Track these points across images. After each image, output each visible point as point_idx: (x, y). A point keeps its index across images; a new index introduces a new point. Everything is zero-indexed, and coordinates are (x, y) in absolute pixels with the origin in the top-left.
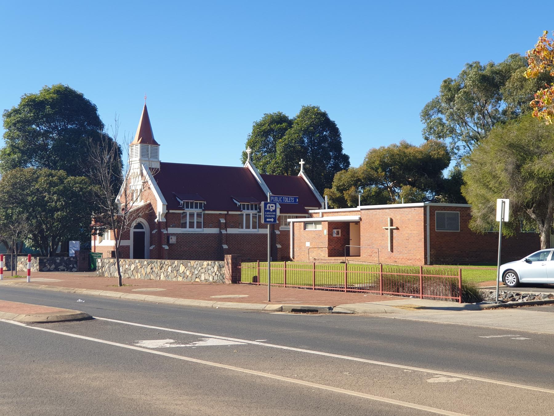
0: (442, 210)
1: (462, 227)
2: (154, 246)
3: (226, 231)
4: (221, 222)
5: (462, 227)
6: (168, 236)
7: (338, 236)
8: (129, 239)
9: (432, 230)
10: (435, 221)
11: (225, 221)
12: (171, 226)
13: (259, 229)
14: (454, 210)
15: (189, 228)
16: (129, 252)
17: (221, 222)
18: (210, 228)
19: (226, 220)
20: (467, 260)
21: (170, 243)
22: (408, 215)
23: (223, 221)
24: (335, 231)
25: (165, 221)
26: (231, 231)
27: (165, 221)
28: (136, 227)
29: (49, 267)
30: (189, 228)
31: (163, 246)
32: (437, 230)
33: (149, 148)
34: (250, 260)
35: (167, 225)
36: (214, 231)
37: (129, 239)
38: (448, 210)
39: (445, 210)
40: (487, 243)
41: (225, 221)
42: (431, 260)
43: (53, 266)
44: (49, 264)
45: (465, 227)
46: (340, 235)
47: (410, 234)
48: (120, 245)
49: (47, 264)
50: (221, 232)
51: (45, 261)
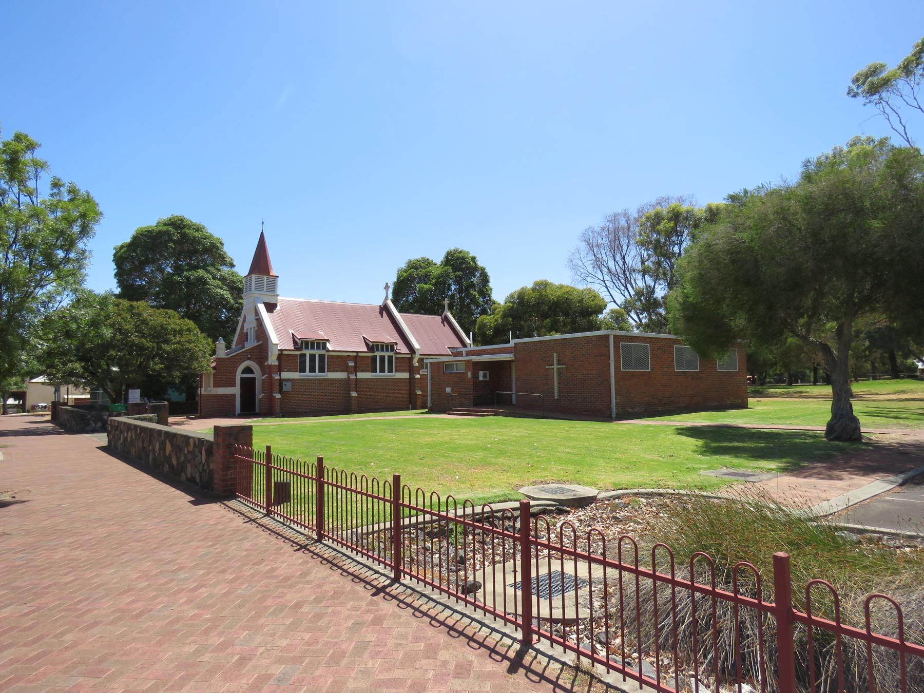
3: (356, 375)
4: (350, 365)
6: (281, 381)
7: (485, 379)
11: (353, 364)
14: (643, 342)
15: (319, 372)
17: (350, 365)
19: (355, 363)
21: (284, 390)
23: (351, 364)
24: (481, 373)
25: (278, 364)
26: (361, 375)
27: (278, 364)
28: (243, 372)
29: (93, 425)
30: (319, 372)
35: (280, 369)
36: (342, 375)
38: (636, 342)
39: (632, 342)
41: (353, 364)
43: (99, 424)
44: (94, 421)
46: (488, 379)
48: (293, 349)
49: (91, 422)
50: (348, 377)
51: (89, 417)
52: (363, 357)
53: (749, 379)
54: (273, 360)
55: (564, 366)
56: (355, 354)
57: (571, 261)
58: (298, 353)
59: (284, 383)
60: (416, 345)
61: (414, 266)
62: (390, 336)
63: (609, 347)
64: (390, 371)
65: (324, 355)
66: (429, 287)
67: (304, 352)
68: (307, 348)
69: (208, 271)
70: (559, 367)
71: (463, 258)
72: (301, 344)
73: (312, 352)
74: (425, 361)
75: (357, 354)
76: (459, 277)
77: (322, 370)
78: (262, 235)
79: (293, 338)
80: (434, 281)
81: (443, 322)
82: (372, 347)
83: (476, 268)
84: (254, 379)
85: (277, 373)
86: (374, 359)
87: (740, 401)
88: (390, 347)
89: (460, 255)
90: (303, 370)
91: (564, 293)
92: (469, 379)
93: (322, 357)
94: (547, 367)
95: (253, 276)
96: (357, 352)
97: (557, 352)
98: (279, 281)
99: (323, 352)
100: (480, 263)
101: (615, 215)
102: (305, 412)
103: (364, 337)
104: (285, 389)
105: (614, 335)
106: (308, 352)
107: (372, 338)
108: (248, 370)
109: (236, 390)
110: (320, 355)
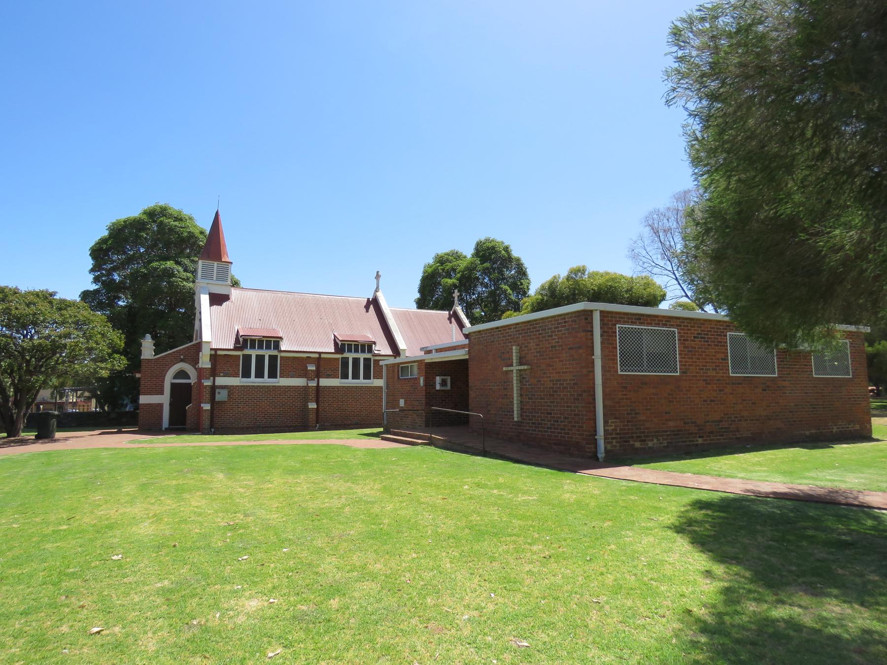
0: (633, 323)
4: (309, 368)
6: (213, 388)
8: (163, 394)
9: (610, 371)
12: (222, 375)
14: (665, 325)
15: (364, 379)
16: (162, 414)
17: (309, 368)
20: (700, 441)
21: (216, 400)
22: (551, 336)
26: (325, 382)
27: (210, 367)
28: (176, 376)
30: (364, 379)
32: (622, 371)
33: (215, 267)
34: (358, 424)
35: (214, 372)
37: (163, 394)
38: (649, 324)
39: (641, 324)
41: (314, 368)
45: (691, 365)
46: (449, 387)
47: (557, 381)
48: (333, 351)
52: (330, 359)
53: (872, 391)
54: (205, 362)
55: (526, 367)
56: (317, 356)
57: (633, 250)
58: (339, 356)
59: (217, 391)
60: (402, 345)
61: (441, 260)
62: (370, 331)
63: (592, 331)
64: (273, 375)
65: (277, 356)
66: (453, 283)
67: (346, 355)
68: (350, 351)
69: (177, 263)
70: (522, 367)
71: (493, 248)
72: (243, 342)
73: (260, 352)
74: (381, 363)
75: (216, 352)
76: (487, 268)
77: (273, 375)
78: (217, 214)
79: (335, 340)
80: (459, 275)
81: (449, 319)
82: (341, 347)
83: (510, 259)
85: (209, 378)
86: (345, 361)
87: (857, 427)
88: (368, 347)
89: (490, 245)
90: (345, 376)
91: (607, 281)
92: (422, 388)
93: (273, 359)
94: (505, 369)
96: (320, 353)
97: (518, 345)
99: (274, 352)
100: (515, 254)
101: (685, 192)
102: (248, 428)
103: (335, 336)
104: (218, 398)
105: (601, 312)
106: (351, 356)
107: (426, 344)
108: (182, 374)
110: (365, 359)
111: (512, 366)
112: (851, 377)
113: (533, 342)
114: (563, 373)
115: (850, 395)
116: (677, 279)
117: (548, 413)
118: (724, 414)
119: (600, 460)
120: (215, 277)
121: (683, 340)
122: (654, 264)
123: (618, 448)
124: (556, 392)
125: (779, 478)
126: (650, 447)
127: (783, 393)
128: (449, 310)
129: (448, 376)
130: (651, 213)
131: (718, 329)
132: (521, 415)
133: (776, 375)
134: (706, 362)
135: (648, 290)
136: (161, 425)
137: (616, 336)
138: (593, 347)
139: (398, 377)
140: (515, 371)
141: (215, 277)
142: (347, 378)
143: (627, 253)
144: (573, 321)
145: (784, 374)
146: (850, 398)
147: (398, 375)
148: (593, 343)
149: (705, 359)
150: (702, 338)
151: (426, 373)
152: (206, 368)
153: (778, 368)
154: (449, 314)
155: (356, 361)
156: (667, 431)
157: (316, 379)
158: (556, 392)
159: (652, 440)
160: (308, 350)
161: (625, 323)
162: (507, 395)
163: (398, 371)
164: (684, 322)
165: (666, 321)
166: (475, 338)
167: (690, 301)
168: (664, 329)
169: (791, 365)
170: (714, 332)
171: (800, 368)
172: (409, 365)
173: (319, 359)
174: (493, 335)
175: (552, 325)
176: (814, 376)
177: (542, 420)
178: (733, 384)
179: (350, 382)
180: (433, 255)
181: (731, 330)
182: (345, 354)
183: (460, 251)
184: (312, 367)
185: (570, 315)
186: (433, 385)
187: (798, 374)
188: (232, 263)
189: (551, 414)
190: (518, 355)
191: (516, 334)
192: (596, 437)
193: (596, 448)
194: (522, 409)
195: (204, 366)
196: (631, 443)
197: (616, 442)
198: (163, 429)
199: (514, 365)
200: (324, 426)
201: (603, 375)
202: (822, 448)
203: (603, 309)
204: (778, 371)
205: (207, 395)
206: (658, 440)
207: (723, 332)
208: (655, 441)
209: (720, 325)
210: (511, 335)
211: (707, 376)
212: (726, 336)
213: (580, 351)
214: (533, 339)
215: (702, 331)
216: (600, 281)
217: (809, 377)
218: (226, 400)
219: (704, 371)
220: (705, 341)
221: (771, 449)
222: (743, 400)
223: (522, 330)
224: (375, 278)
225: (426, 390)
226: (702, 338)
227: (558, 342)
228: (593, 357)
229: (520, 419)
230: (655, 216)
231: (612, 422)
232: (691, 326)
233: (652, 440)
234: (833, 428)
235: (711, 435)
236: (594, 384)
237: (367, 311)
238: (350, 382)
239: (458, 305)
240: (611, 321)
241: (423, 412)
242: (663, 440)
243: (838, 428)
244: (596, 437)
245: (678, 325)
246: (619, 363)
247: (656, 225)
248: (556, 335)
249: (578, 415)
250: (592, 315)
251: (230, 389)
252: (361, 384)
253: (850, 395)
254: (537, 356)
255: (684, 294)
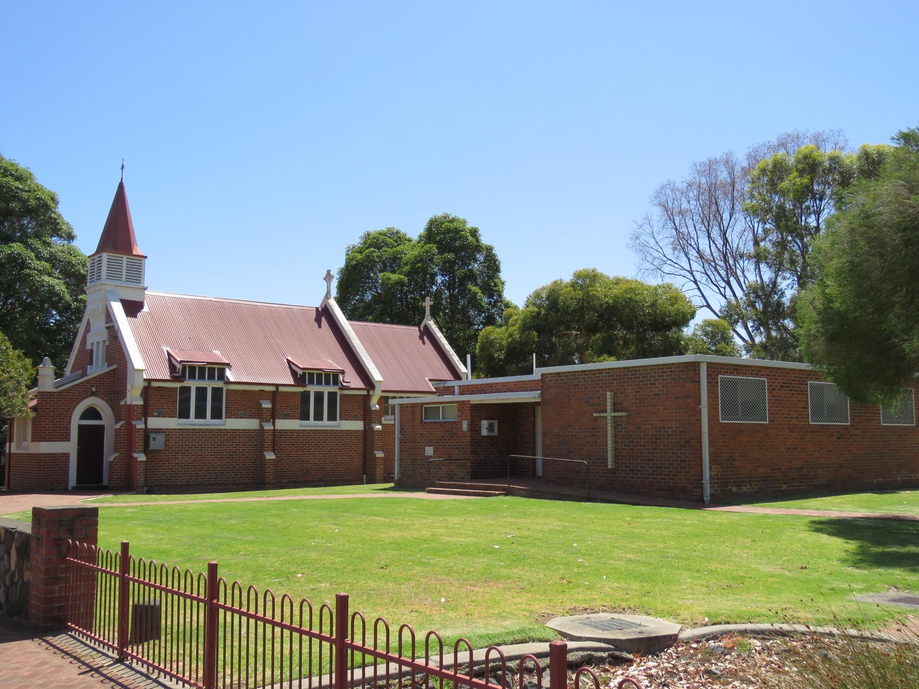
0: (732, 373)
1: (773, 414)
2: (117, 454)
4: (264, 406)
5: (773, 414)
6: (147, 432)
7: (491, 434)
8: (69, 441)
10: (718, 398)
12: (155, 414)
13: (227, 419)
14: (757, 375)
16: (68, 467)
17: (264, 406)
18: (241, 418)
20: (784, 487)
22: (655, 384)
23: (267, 405)
25: (141, 403)
26: (283, 424)
28: (84, 416)
31: (135, 455)
32: (722, 419)
33: (125, 263)
35: (146, 412)
36: (250, 424)
37: (69, 441)
38: (744, 374)
39: (738, 374)
40: (820, 448)
41: (270, 406)
42: (713, 489)
45: (777, 414)
46: (496, 433)
48: (169, 378)
50: (261, 427)
54: (134, 397)
55: (623, 414)
56: (273, 389)
57: (637, 238)
58: (177, 385)
59: (152, 435)
61: (374, 242)
63: (699, 382)
64: (332, 417)
68: (192, 377)
69: (28, 246)
70: (616, 414)
74: (391, 402)
77: (216, 414)
78: (121, 187)
79: (170, 360)
80: (407, 268)
81: (421, 337)
83: (478, 248)
84: (101, 428)
85: (140, 419)
86: (305, 396)
88: (333, 377)
90: (185, 414)
91: (626, 291)
92: (465, 433)
93: (217, 392)
94: (595, 415)
95: (105, 256)
96: (277, 386)
97: (612, 391)
98: (148, 266)
99: (219, 384)
104: (153, 445)
108: (92, 413)
109: (70, 447)
111: (606, 412)
112: (914, 425)
113: (632, 389)
114: (668, 420)
115: (914, 444)
116: (695, 282)
117: (649, 460)
118: (805, 462)
119: (706, 503)
120: (124, 277)
121: (772, 390)
122: (665, 259)
123: (719, 492)
124: (659, 439)
125: (862, 510)
126: (744, 492)
127: (855, 441)
128: (419, 325)
129: (496, 419)
130: (663, 187)
131: (800, 377)
132: (616, 463)
133: (849, 424)
134: (790, 411)
135: (676, 306)
136: (67, 483)
137: (718, 387)
138: (700, 397)
139: (422, 420)
140: (609, 418)
141: (124, 277)
142: (308, 419)
143: (630, 242)
144: (680, 371)
145: (856, 422)
146: (913, 447)
147: (422, 418)
148: (700, 393)
149: (789, 407)
150: (787, 387)
151: (471, 416)
152: (137, 405)
153: (851, 416)
154: (420, 330)
155: (319, 396)
156: (757, 477)
157: (143, 419)
158: (659, 439)
159: (746, 486)
160: (262, 382)
161: (725, 373)
162: (596, 442)
163: (422, 412)
164: (772, 372)
165: (758, 371)
166: (552, 380)
167: (717, 318)
168: (756, 378)
169: (862, 413)
170: (798, 381)
171: (869, 416)
172: (441, 406)
173: (275, 393)
174: (578, 378)
175: (655, 373)
176: (882, 424)
177: (642, 467)
178: (812, 432)
179: (312, 424)
180: (362, 233)
181: (811, 379)
182: (185, 382)
183: (403, 231)
184: (267, 405)
185: (676, 365)
186: (478, 431)
187: (868, 423)
188: (146, 257)
189: (653, 460)
190: (612, 400)
191: (609, 380)
192: (703, 482)
193: (702, 491)
194: (616, 456)
195: (134, 403)
196: (730, 487)
197: (718, 487)
198: (70, 488)
199: (609, 411)
200: (281, 483)
201: (709, 424)
202: (890, 493)
203: (709, 361)
204: (851, 419)
205: (139, 442)
206: (751, 485)
207: (804, 381)
208: (748, 486)
209: (803, 374)
210: (601, 380)
211: (790, 425)
212: (807, 384)
213: (689, 401)
214: (631, 385)
215: (787, 380)
216: (616, 291)
217: (877, 426)
218: (163, 448)
219: (789, 419)
220: (789, 390)
221: (847, 494)
222: (820, 448)
223: (618, 376)
224: (325, 279)
225: (471, 436)
226: (787, 387)
227: (663, 390)
228: (700, 406)
229: (614, 467)
230: (669, 192)
231: (715, 468)
232: (779, 376)
233: (746, 486)
234: (897, 477)
235: (794, 481)
236: (701, 431)
237: (320, 326)
238: (312, 424)
239: (430, 317)
240: (714, 372)
241: (468, 461)
242: (755, 485)
243: (901, 477)
244: (703, 482)
245: (767, 375)
246: (720, 412)
247: (670, 205)
248: (660, 383)
249: (685, 461)
250: (699, 366)
251: (167, 433)
252: (311, 426)
253: (914, 444)
254: (636, 403)
255: (705, 304)
